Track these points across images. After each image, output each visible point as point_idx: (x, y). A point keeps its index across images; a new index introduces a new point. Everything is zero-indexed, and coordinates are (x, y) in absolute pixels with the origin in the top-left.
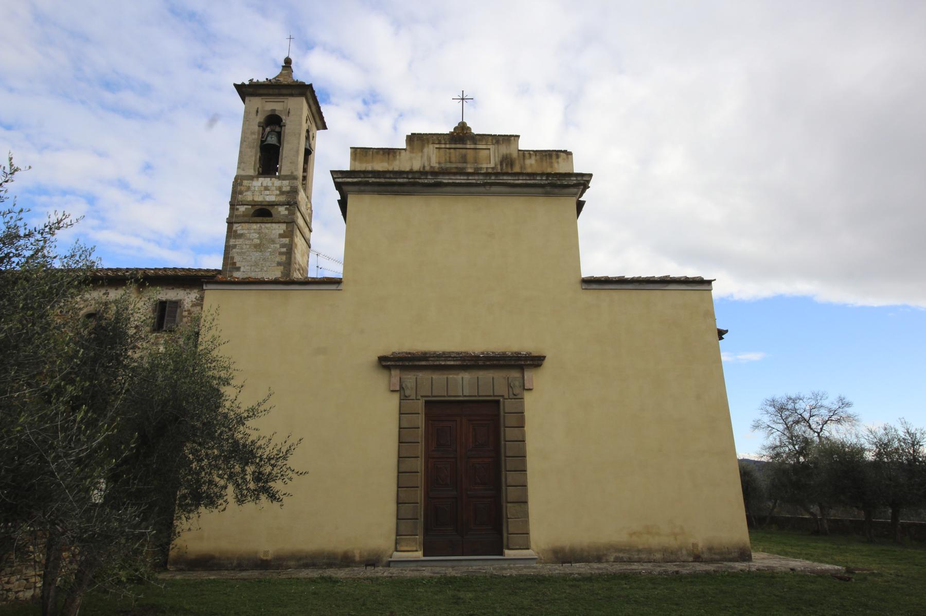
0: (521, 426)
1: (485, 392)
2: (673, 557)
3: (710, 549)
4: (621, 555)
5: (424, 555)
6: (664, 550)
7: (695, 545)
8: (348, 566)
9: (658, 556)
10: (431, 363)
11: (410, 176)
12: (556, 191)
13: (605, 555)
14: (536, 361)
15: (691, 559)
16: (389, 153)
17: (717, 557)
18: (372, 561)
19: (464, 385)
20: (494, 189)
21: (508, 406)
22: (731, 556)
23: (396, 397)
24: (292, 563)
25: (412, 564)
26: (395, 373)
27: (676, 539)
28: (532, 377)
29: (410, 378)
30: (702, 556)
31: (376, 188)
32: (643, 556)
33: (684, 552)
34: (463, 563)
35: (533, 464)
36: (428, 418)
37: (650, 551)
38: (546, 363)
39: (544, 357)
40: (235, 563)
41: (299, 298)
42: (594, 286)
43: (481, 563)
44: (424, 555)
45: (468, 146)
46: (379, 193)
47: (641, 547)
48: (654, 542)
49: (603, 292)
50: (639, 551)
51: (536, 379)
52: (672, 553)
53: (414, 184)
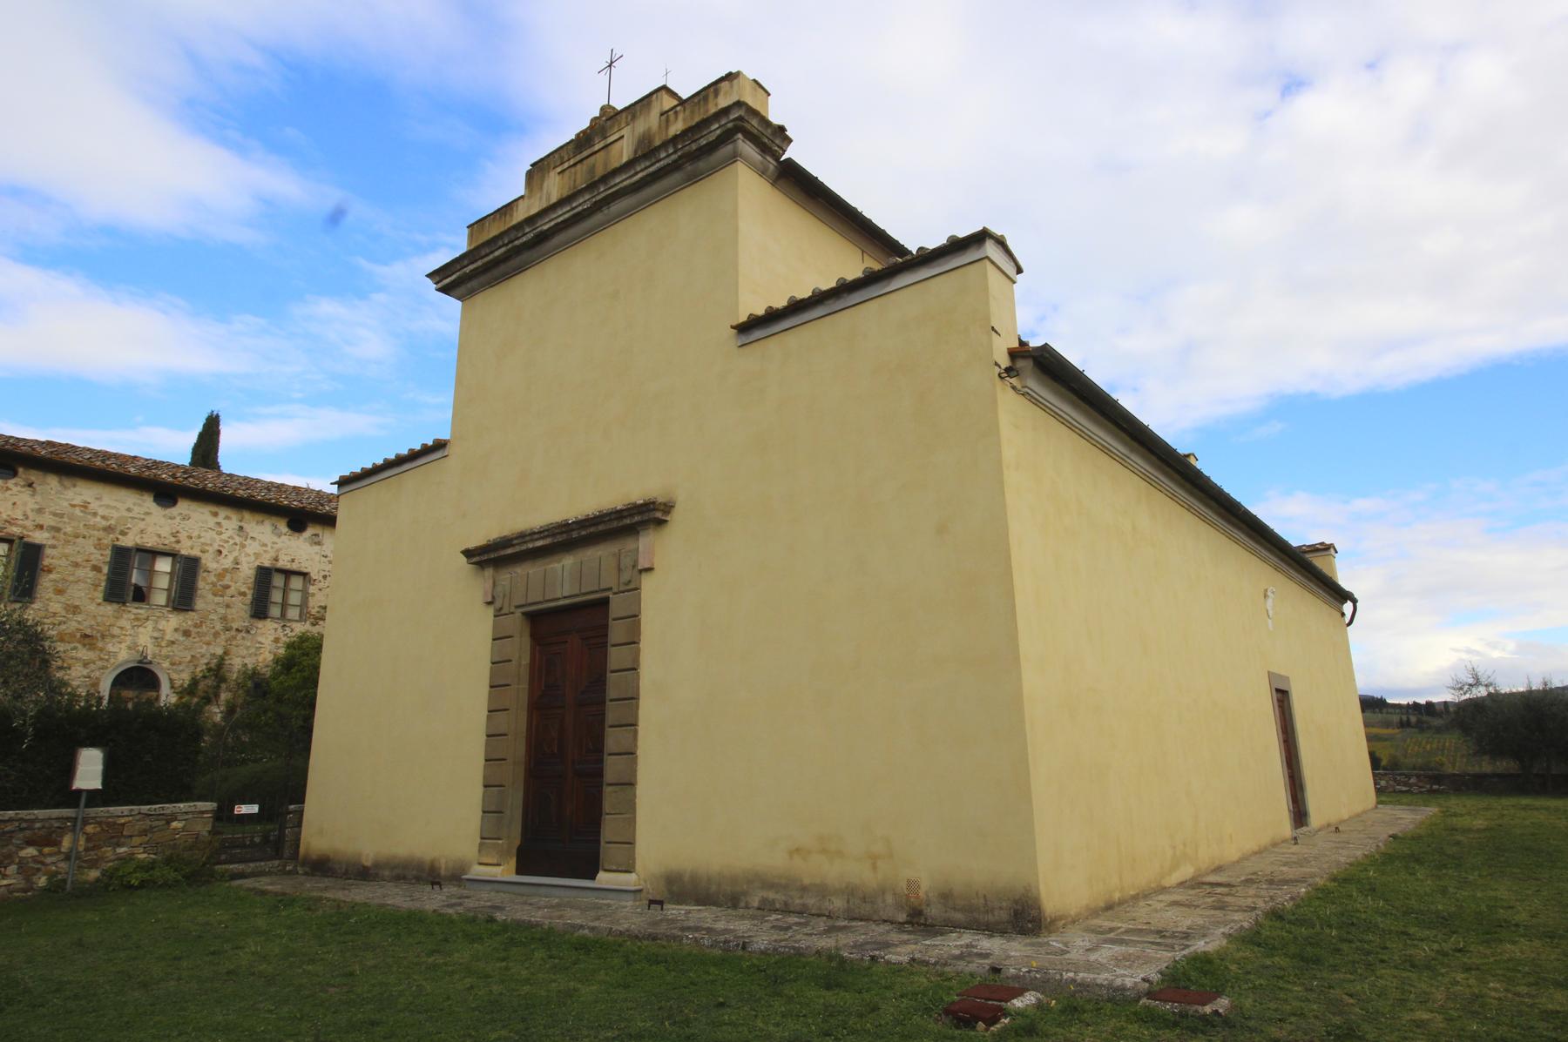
0: (633, 641)
1: (588, 589)
2: (866, 909)
3: (946, 896)
4: (771, 895)
5: (519, 872)
6: (850, 891)
7: (912, 884)
8: (1023, 932)
9: (838, 904)
10: (517, 549)
11: (663, 155)
12: (701, 164)
13: (745, 894)
14: (645, 516)
15: (902, 917)
16: (508, 208)
17: (959, 916)
18: (428, 875)
19: (563, 578)
20: (616, 207)
21: (617, 607)
22: (990, 918)
23: (491, 611)
24: (387, 873)
25: (488, 887)
26: (489, 572)
27: (874, 867)
28: (649, 544)
29: (506, 576)
30: (927, 911)
31: (483, 279)
32: (811, 901)
33: (890, 899)
34: (542, 890)
35: (649, 712)
36: (536, 638)
37: (823, 891)
38: (676, 517)
39: (668, 507)
40: (1004, 916)
41: (906, 301)
42: (758, 334)
43: (574, 893)
44: (519, 872)
45: (597, 148)
46: (491, 284)
47: (807, 881)
48: (832, 871)
49: (772, 344)
50: (804, 889)
51: (662, 550)
52: (864, 900)
53: (518, 251)
